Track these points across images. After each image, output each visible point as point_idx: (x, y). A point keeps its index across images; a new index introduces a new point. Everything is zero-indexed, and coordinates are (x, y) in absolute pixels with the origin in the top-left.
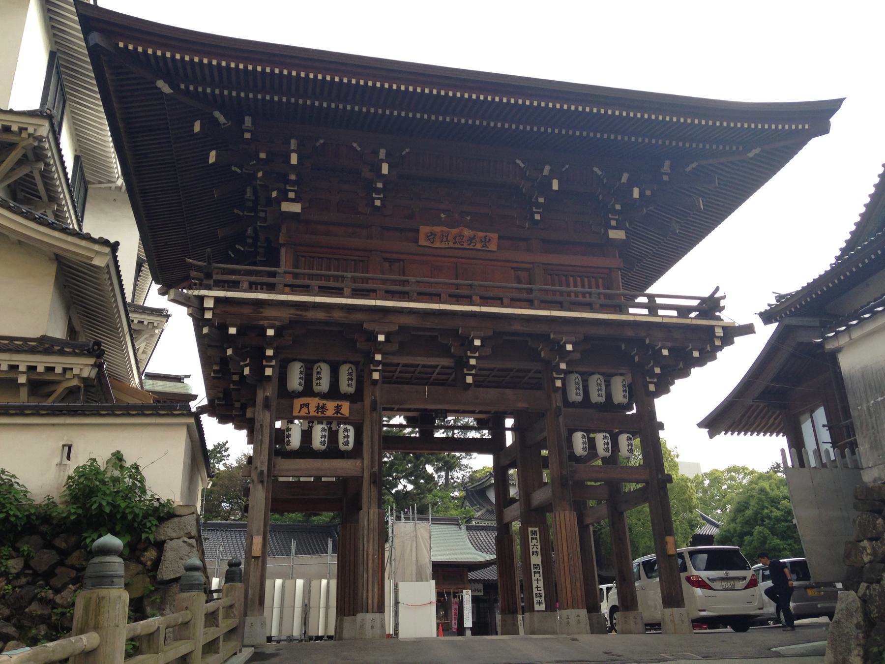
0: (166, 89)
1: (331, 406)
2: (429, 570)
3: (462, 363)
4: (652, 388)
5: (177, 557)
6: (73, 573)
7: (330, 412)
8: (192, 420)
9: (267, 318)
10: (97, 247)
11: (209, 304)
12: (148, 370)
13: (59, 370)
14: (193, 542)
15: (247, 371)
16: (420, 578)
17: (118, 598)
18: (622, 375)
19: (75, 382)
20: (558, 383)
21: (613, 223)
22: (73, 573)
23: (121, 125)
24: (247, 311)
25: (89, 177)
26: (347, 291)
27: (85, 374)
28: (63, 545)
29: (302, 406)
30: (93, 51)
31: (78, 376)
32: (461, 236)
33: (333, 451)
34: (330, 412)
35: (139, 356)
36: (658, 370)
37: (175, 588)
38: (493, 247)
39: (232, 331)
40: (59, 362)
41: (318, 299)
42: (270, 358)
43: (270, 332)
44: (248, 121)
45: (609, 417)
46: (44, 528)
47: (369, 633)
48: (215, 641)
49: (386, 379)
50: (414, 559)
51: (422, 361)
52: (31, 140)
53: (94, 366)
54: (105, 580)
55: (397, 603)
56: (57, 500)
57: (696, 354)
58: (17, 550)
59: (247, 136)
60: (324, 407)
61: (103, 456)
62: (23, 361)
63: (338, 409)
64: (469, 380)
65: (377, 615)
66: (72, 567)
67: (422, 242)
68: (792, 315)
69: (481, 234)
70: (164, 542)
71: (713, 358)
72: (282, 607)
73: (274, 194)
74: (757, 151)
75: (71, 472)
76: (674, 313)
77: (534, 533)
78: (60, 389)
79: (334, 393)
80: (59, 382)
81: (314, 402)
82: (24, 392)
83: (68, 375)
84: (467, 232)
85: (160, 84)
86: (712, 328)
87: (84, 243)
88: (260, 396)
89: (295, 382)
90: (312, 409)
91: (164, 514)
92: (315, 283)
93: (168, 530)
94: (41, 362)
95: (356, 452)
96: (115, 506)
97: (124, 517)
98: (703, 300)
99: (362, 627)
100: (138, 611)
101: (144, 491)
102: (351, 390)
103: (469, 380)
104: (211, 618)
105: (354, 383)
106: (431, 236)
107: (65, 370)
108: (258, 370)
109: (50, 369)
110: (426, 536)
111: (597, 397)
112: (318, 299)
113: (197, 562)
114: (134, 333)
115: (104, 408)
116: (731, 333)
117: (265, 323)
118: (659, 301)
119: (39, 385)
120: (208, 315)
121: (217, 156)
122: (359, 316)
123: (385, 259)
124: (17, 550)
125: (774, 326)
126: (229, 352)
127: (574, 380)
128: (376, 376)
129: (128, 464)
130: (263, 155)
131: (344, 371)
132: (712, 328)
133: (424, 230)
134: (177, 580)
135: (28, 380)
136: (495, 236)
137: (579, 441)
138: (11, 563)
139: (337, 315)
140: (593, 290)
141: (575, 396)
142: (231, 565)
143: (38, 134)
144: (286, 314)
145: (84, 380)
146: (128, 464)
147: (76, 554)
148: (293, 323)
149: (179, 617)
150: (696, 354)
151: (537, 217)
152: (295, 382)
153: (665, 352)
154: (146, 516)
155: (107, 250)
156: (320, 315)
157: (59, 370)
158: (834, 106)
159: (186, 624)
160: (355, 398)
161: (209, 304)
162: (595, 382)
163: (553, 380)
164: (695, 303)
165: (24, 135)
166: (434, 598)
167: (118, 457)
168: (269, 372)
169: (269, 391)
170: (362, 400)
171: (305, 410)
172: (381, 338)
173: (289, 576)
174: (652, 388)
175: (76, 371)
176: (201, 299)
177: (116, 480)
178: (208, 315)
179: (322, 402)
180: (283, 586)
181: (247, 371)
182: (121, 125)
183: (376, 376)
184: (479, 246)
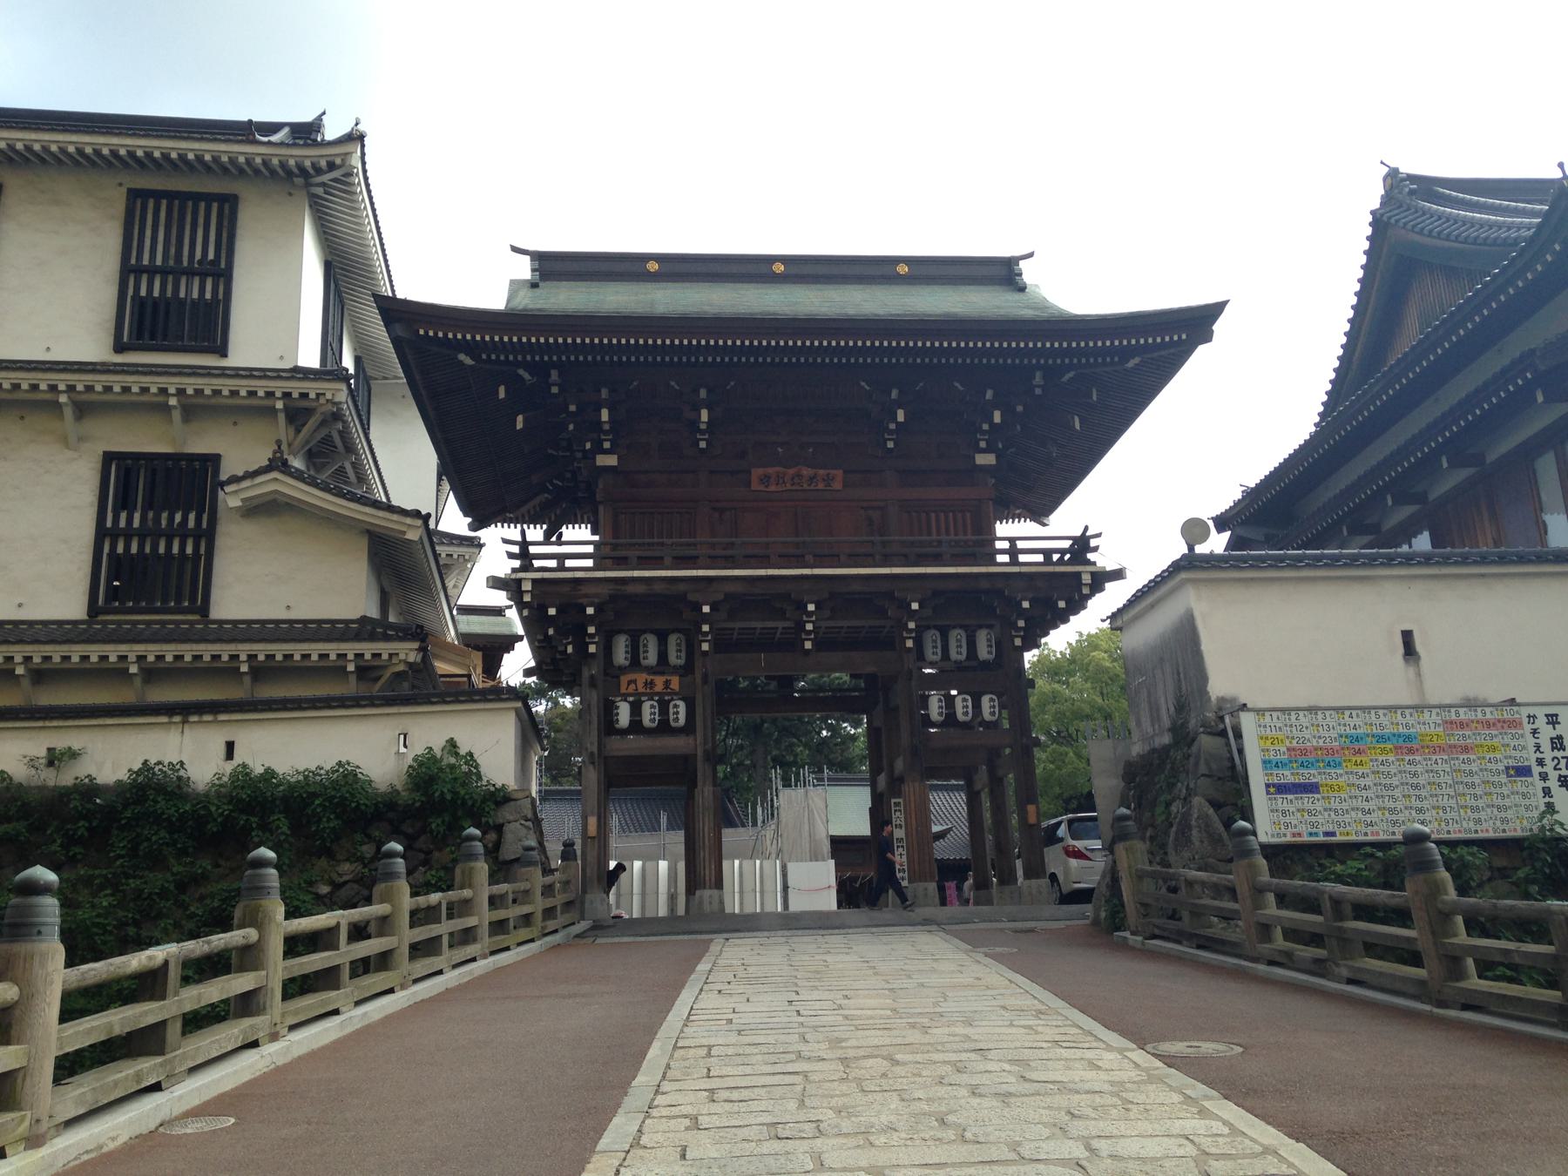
0: (468, 361)
1: (659, 681)
2: (826, 847)
3: (800, 626)
4: (1018, 642)
5: (518, 838)
6: (422, 856)
8: (519, 704)
9: (586, 596)
10: (408, 521)
11: (527, 586)
12: (462, 601)
13: (385, 656)
14: (529, 824)
15: (570, 649)
16: (815, 857)
17: (482, 868)
18: (990, 627)
19: (401, 667)
21: (983, 444)
22: (422, 856)
23: (418, 377)
24: (566, 589)
25: (370, 372)
26: (668, 560)
27: (411, 659)
28: (410, 831)
29: (629, 683)
30: (397, 342)
31: (405, 662)
32: (799, 476)
33: (664, 727)
34: (659, 687)
35: (450, 592)
37: (516, 865)
38: (837, 485)
39: (552, 611)
40: (384, 648)
41: (636, 574)
42: (592, 636)
43: (590, 611)
44: (554, 375)
46: (391, 815)
47: (707, 908)
48: (553, 909)
49: (718, 646)
50: (806, 834)
51: (759, 625)
52: (330, 407)
53: (420, 649)
54: (472, 856)
55: (785, 888)
56: (399, 787)
57: (1062, 604)
58: (368, 836)
59: (555, 390)
60: (652, 682)
61: (438, 744)
62: (351, 649)
64: (808, 645)
65: (716, 892)
66: (421, 850)
67: (755, 486)
68: (1243, 523)
69: (822, 472)
70: (502, 825)
72: (643, 894)
73: (588, 446)
74: (1137, 360)
75: (410, 761)
76: (1040, 558)
77: (897, 804)
78: (387, 674)
80: (385, 667)
81: (641, 678)
82: (353, 679)
83: (394, 661)
84: (807, 472)
85: (462, 357)
86: (1078, 575)
87: (395, 517)
88: (586, 674)
89: (621, 656)
91: (500, 798)
92: (633, 554)
93: (506, 813)
94: (368, 649)
95: (689, 729)
96: (455, 793)
97: (464, 803)
99: (701, 903)
100: (494, 879)
101: (479, 777)
102: (681, 662)
103: (808, 645)
104: (548, 890)
105: (683, 655)
106: (765, 479)
107: (391, 655)
108: (582, 647)
109: (376, 656)
110: (822, 805)
112: (636, 574)
113: (533, 843)
114: (443, 570)
115: (435, 695)
116: (1101, 579)
117: (584, 601)
118: (1020, 545)
119: (366, 671)
120: (527, 598)
122: (682, 587)
123: (714, 509)
124: (368, 836)
125: (1228, 534)
126: (551, 632)
127: (932, 637)
128: (705, 647)
129: (463, 752)
130: (573, 408)
131: (673, 640)
132: (1078, 575)
133: (757, 472)
134: (517, 860)
135: (357, 667)
136: (839, 473)
138: (365, 848)
139: (658, 588)
140: (944, 537)
142: (565, 845)
143: (337, 399)
144: (605, 590)
145: (410, 665)
146: (463, 752)
147: (423, 838)
148: (613, 598)
149: (522, 886)
152: (621, 656)
154: (484, 801)
155: (419, 522)
156: (640, 589)
157: (385, 656)
158: (1215, 310)
159: (526, 892)
160: (686, 670)
162: (957, 637)
164: (1066, 544)
165: (322, 401)
166: (833, 882)
167: (452, 744)
168: (592, 649)
169: (594, 669)
170: (693, 673)
171: (633, 686)
172: (706, 609)
173: (650, 857)
174: (1018, 642)
175: (402, 656)
177: (452, 767)
178: (527, 598)
179: (650, 678)
180: (643, 869)
181: (570, 649)
182: (418, 377)
183: (705, 647)
184: (821, 486)
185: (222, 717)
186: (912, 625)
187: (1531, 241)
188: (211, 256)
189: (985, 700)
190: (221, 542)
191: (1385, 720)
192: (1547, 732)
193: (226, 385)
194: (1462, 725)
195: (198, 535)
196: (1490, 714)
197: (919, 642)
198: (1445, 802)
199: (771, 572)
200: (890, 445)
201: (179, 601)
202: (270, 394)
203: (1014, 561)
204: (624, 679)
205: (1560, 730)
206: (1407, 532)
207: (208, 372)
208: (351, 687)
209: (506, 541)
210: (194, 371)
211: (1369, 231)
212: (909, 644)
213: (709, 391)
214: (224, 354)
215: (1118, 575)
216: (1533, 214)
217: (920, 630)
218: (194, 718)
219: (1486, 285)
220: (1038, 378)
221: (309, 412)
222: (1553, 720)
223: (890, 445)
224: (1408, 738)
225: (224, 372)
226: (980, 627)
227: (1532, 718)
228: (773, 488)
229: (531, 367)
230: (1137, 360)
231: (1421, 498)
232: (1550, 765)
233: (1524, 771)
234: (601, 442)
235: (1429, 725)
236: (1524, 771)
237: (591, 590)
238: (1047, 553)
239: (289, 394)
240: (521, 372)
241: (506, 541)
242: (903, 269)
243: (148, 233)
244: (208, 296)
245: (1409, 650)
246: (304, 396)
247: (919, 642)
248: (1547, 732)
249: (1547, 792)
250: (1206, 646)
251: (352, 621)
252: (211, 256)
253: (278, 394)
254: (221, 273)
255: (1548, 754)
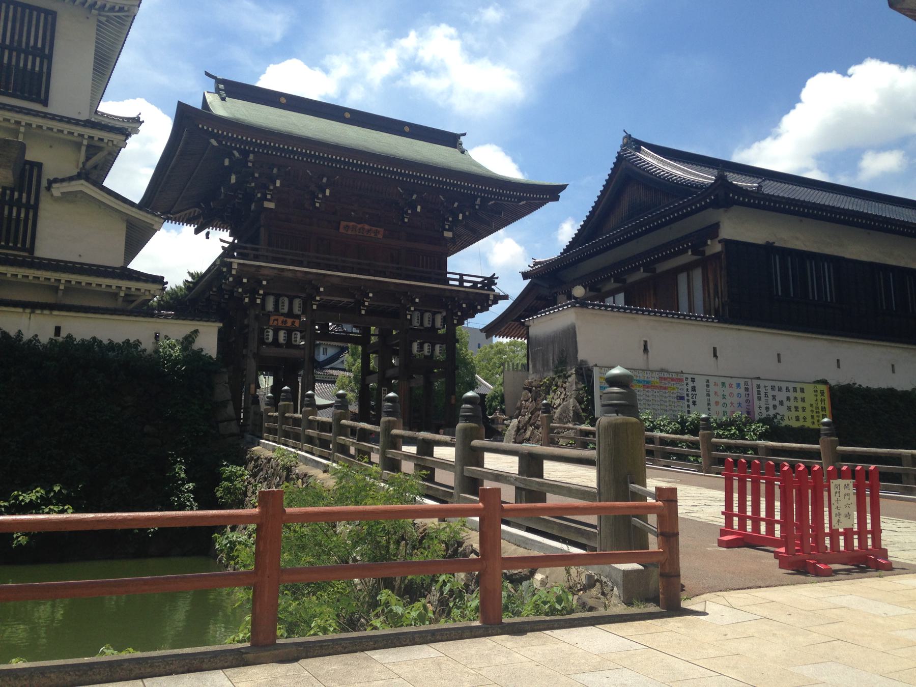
1: (290, 321)
4: (455, 322)
7: (289, 324)
20: (409, 317)
21: (447, 227)
32: (363, 229)
34: (289, 324)
36: (459, 314)
38: (380, 236)
41: (291, 268)
44: (251, 157)
45: (429, 335)
57: (479, 307)
63: (293, 323)
64: (363, 312)
67: (342, 230)
71: (488, 310)
74: (524, 202)
79: (290, 314)
84: (367, 227)
89: (270, 306)
90: (280, 322)
98: (486, 278)
103: (363, 312)
108: (253, 300)
111: (427, 324)
116: (498, 298)
118: (465, 278)
121: (236, 179)
125: (528, 281)
133: (343, 224)
136: (381, 230)
137: (415, 346)
139: (299, 275)
141: (416, 323)
150: (479, 307)
151: (406, 220)
152: (270, 306)
153: (464, 306)
156: (290, 275)
158: (563, 187)
161: (235, 266)
163: (406, 315)
164: (480, 280)
174: (455, 322)
176: (231, 263)
184: (373, 235)
185: (55, 313)
186: (261, 292)
187: (708, 188)
188: (39, 45)
189: (438, 347)
190: (42, 214)
191: (641, 375)
192: (691, 384)
193: (46, 123)
194: (665, 379)
195: (28, 207)
196: (674, 376)
197: (263, 301)
198: (656, 407)
199: (356, 276)
200: (317, 205)
201: (7, 242)
202: (81, 136)
203: (461, 285)
204: (272, 318)
205: (695, 384)
206: (613, 293)
207: (37, 114)
208: (120, 304)
209: (222, 240)
210: (29, 112)
211: (615, 160)
212: (258, 301)
213: (279, 170)
214: (45, 103)
215: (506, 297)
216: (710, 179)
217: (265, 294)
218: (38, 311)
219: (680, 204)
220: (478, 201)
221: (100, 149)
222: (693, 380)
223: (317, 205)
224: (648, 382)
225: (45, 116)
226: (426, 311)
227: (687, 378)
228: (350, 232)
229: (240, 151)
230: (524, 202)
231: (624, 281)
232: (690, 396)
233: (682, 398)
234: (266, 195)
235: (654, 378)
236: (682, 398)
237: (266, 272)
238: (475, 283)
239: (30, 125)
240: (235, 152)
241: (222, 240)
242: (283, 100)
243: (25, 29)
244: (37, 69)
245: (646, 349)
246: (101, 140)
247: (263, 301)
248: (691, 384)
249: (688, 406)
250: (579, 339)
251: (117, 268)
252: (39, 45)
253: (23, 124)
254: (47, 58)
255: (690, 392)
